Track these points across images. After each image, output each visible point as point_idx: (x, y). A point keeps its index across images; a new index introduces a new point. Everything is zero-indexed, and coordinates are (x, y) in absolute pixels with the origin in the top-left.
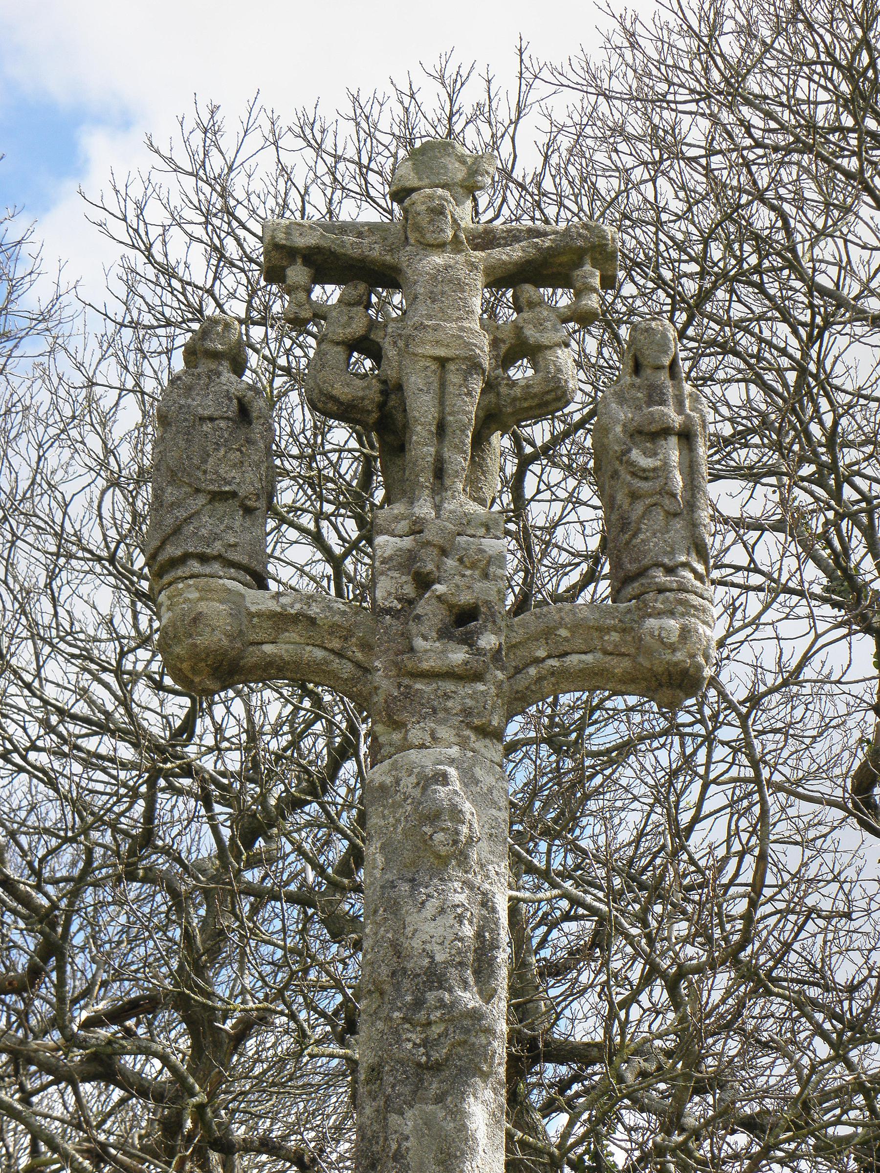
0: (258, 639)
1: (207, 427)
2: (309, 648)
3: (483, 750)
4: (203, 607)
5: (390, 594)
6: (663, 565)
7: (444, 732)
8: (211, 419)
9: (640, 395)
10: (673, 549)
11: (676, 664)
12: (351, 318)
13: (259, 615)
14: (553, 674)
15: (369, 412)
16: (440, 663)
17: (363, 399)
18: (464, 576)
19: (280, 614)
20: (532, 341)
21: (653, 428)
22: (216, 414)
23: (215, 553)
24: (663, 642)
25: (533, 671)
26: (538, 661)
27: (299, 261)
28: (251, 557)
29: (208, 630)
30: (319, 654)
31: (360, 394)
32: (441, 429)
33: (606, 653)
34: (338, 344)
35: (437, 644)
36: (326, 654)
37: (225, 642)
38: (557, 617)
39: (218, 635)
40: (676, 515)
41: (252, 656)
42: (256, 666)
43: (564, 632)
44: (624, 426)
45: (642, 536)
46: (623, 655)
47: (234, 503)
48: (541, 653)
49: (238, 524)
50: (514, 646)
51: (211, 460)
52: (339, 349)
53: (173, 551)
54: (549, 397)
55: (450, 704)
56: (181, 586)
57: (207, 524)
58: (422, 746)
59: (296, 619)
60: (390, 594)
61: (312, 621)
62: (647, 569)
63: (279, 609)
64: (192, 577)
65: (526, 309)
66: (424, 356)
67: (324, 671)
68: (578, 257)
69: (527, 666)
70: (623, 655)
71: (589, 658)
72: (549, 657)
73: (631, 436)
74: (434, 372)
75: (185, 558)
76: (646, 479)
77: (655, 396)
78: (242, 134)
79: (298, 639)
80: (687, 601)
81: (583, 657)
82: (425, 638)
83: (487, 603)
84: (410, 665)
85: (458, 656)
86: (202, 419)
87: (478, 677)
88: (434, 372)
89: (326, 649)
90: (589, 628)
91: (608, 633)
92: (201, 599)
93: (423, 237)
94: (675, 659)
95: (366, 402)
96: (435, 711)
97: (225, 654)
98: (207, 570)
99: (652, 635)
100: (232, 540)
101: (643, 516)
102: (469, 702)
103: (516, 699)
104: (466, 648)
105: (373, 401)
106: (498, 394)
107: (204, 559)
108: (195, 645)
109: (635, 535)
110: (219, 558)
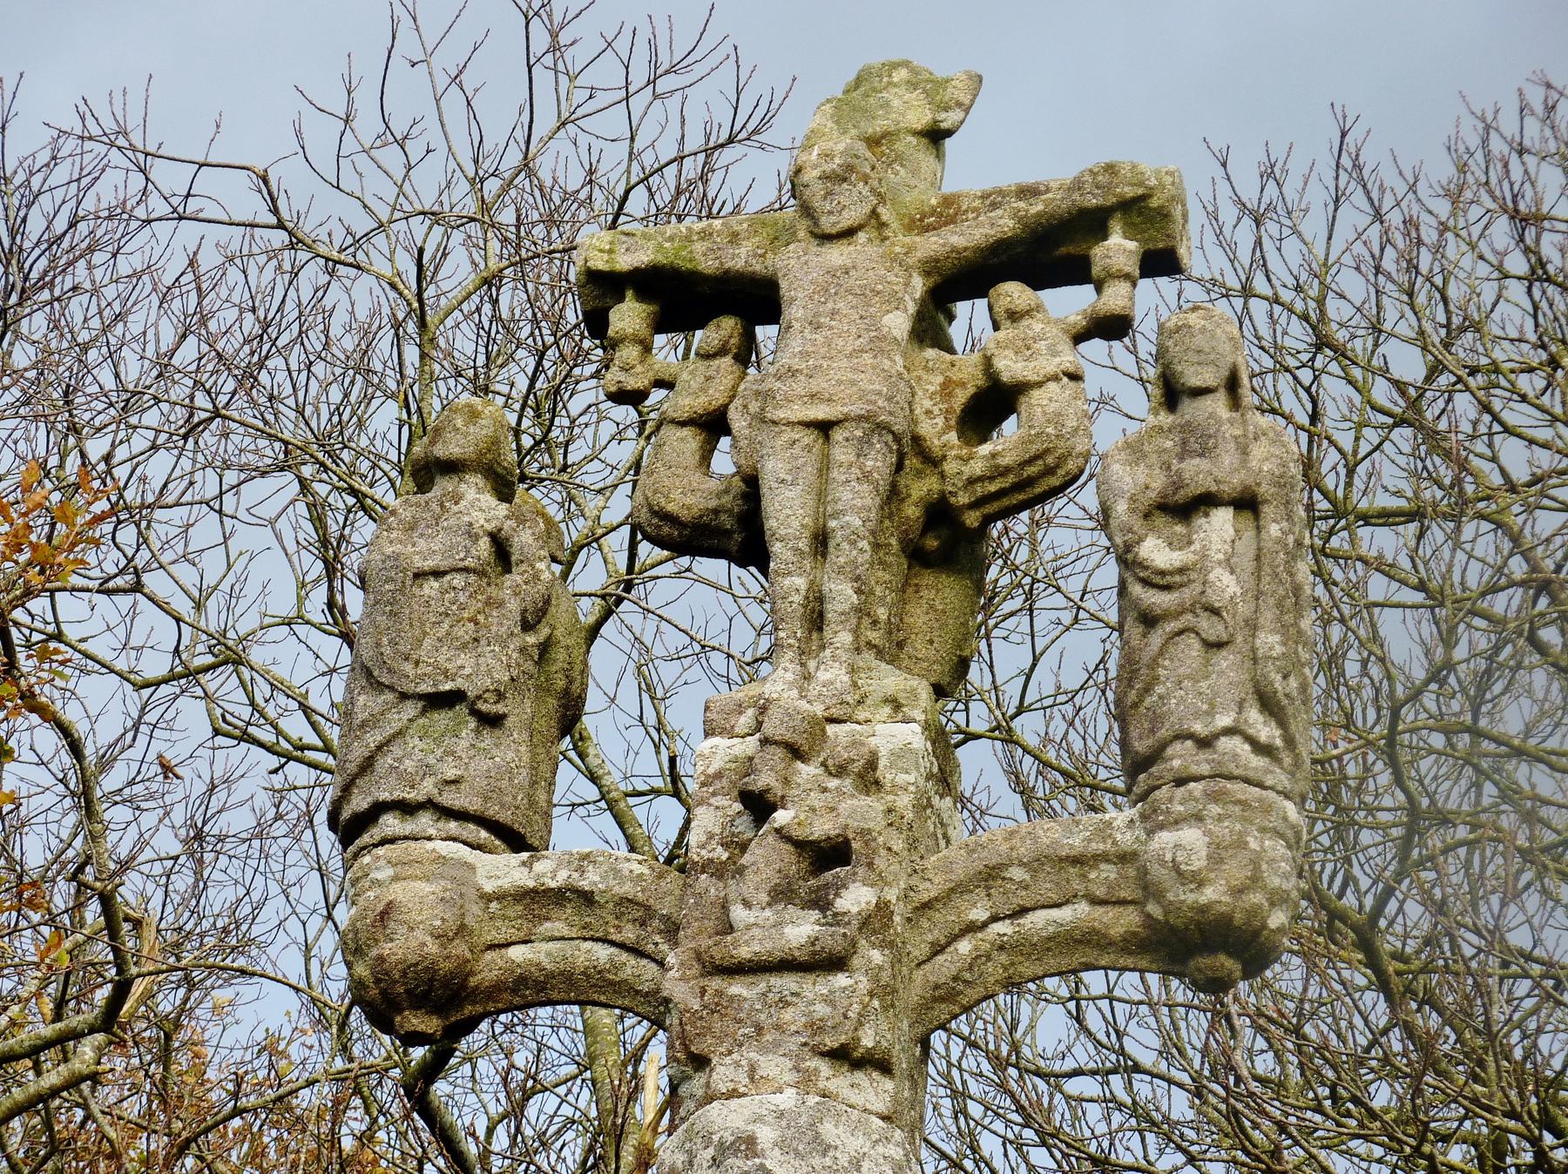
0: (500, 938)
1: (431, 587)
2: (588, 945)
3: (846, 1093)
4: (397, 892)
5: (711, 836)
6: (1191, 736)
7: (774, 1066)
8: (437, 574)
9: (1169, 444)
10: (1212, 706)
11: (1203, 909)
12: (708, 379)
13: (500, 897)
14: (1001, 948)
15: (728, 533)
16: (769, 945)
17: (716, 512)
18: (825, 790)
19: (534, 891)
20: (1005, 377)
21: (1181, 497)
22: (444, 565)
23: (421, 798)
24: (1180, 873)
25: (964, 946)
26: (972, 928)
27: (629, 294)
28: (486, 799)
29: (403, 930)
30: (603, 953)
31: (713, 504)
32: (821, 541)
33: (1095, 901)
34: (683, 424)
35: (768, 913)
36: (613, 950)
37: (433, 948)
38: (1004, 847)
39: (421, 935)
40: (1219, 645)
41: (489, 968)
42: (497, 988)
43: (1017, 873)
44: (1133, 499)
45: (1160, 689)
46: (1122, 902)
47: (461, 709)
48: (979, 914)
49: (464, 744)
50: (926, 906)
51: (427, 642)
52: (686, 432)
53: (359, 802)
54: (1031, 470)
55: (788, 1015)
56: (367, 859)
57: (413, 753)
58: (733, 1094)
59: (558, 897)
60: (711, 836)
61: (587, 898)
62: (1164, 745)
63: (531, 884)
64: (384, 842)
65: (1006, 324)
66: (789, 424)
67: (612, 983)
68: (1093, 223)
69: (954, 938)
70: (1122, 902)
71: (1065, 914)
72: (995, 919)
73: (1147, 516)
74: (809, 449)
75: (379, 809)
76: (1167, 588)
77: (1196, 442)
78: (1331, 207)
79: (566, 932)
80: (1225, 793)
81: (1055, 914)
82: (747, 904)
83: (864, 833)
84: (717, 953)
85: (801, 930)
86: (419, 575)
87: (835, 963)
88: (809, 449)
89: (613, 943)
90: (1061, 860)
91: (1094, 867)
92: (396, 878)
93: (816, 224)
94: (1203, 900)
95: (723, 517)
96: (759, 1029)
97: (431, 970)
98: (408, 827)
99: (1162, 863)
100: (451, 773)
101: (1161, 653)
102: (821, 1010)
103: (935, 1000)
104: (815, 915)
105: (730, 511)
106: (943, 476)
107: (407, 809)
108: (381, 959)
109: (1147, 690)
110: (429, 804)
